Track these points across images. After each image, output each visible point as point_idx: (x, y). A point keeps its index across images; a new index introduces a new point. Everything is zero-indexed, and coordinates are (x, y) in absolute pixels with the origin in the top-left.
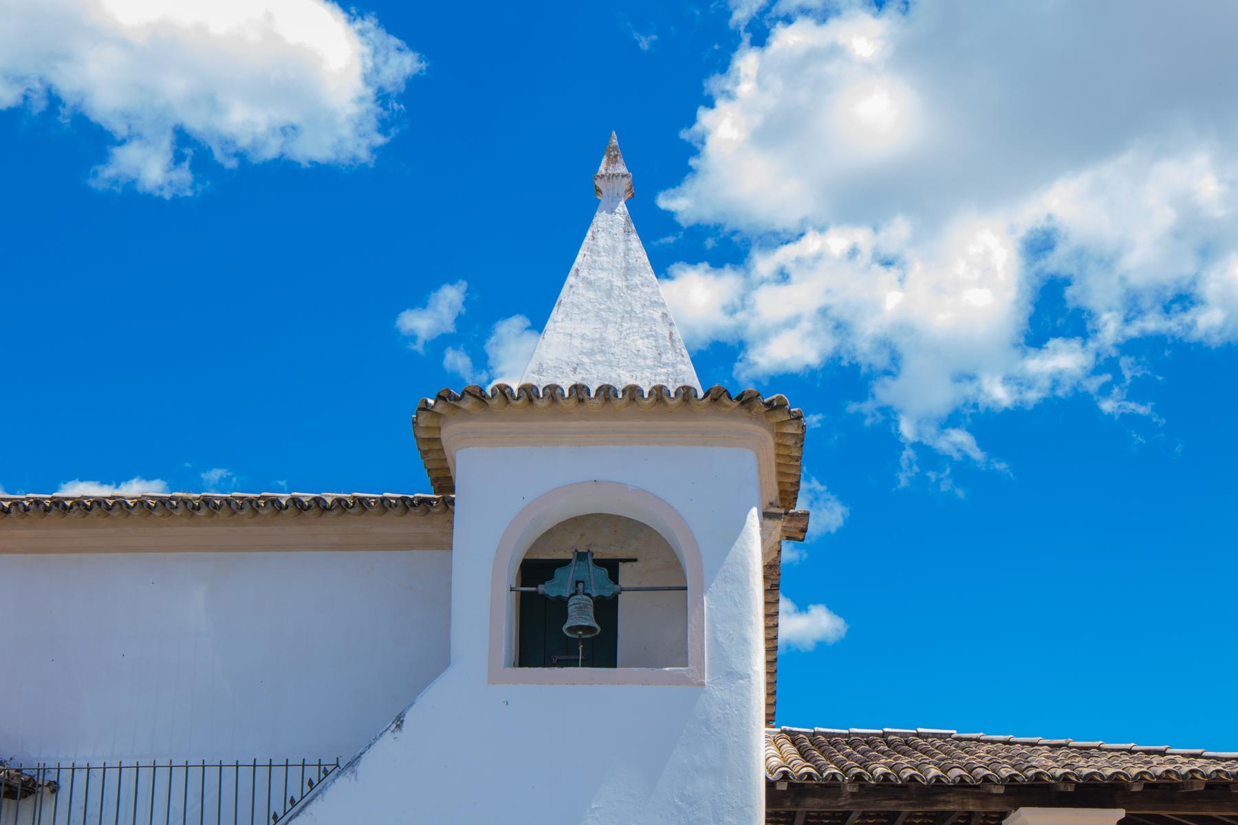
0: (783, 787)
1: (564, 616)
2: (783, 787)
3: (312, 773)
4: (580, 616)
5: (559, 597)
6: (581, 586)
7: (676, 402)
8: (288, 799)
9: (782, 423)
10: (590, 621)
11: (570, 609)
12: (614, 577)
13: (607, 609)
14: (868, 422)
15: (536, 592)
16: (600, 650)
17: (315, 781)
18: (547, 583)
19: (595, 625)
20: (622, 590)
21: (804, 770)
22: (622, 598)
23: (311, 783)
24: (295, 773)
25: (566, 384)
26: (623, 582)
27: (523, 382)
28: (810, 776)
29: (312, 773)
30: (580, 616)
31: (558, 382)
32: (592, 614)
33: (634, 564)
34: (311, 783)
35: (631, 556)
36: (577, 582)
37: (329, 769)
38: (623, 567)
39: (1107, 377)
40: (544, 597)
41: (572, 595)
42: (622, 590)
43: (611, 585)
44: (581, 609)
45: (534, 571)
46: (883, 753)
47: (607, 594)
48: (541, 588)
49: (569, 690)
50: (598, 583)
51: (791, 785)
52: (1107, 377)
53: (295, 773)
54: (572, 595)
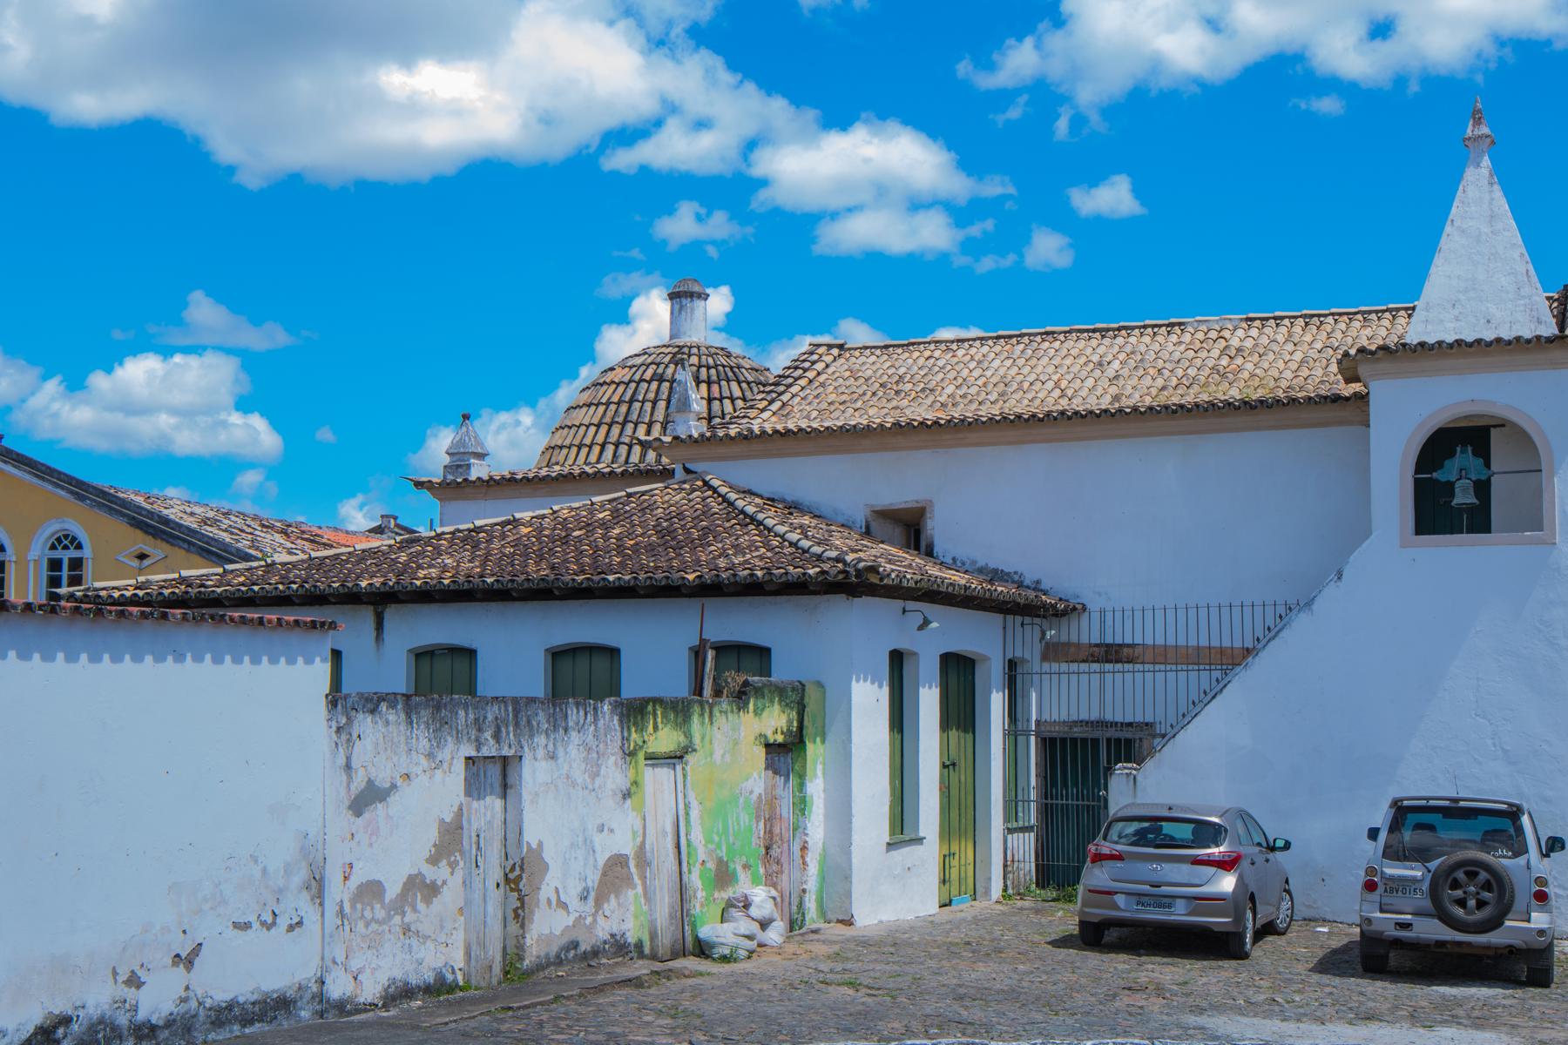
1: (1452, 495)
12: (1488, 465)
13: (1483, 489)
16: (1478, 520)
40: (1436, 481)
43: (1485, 471)
44: (1465, 490)
47: (1483, 478)
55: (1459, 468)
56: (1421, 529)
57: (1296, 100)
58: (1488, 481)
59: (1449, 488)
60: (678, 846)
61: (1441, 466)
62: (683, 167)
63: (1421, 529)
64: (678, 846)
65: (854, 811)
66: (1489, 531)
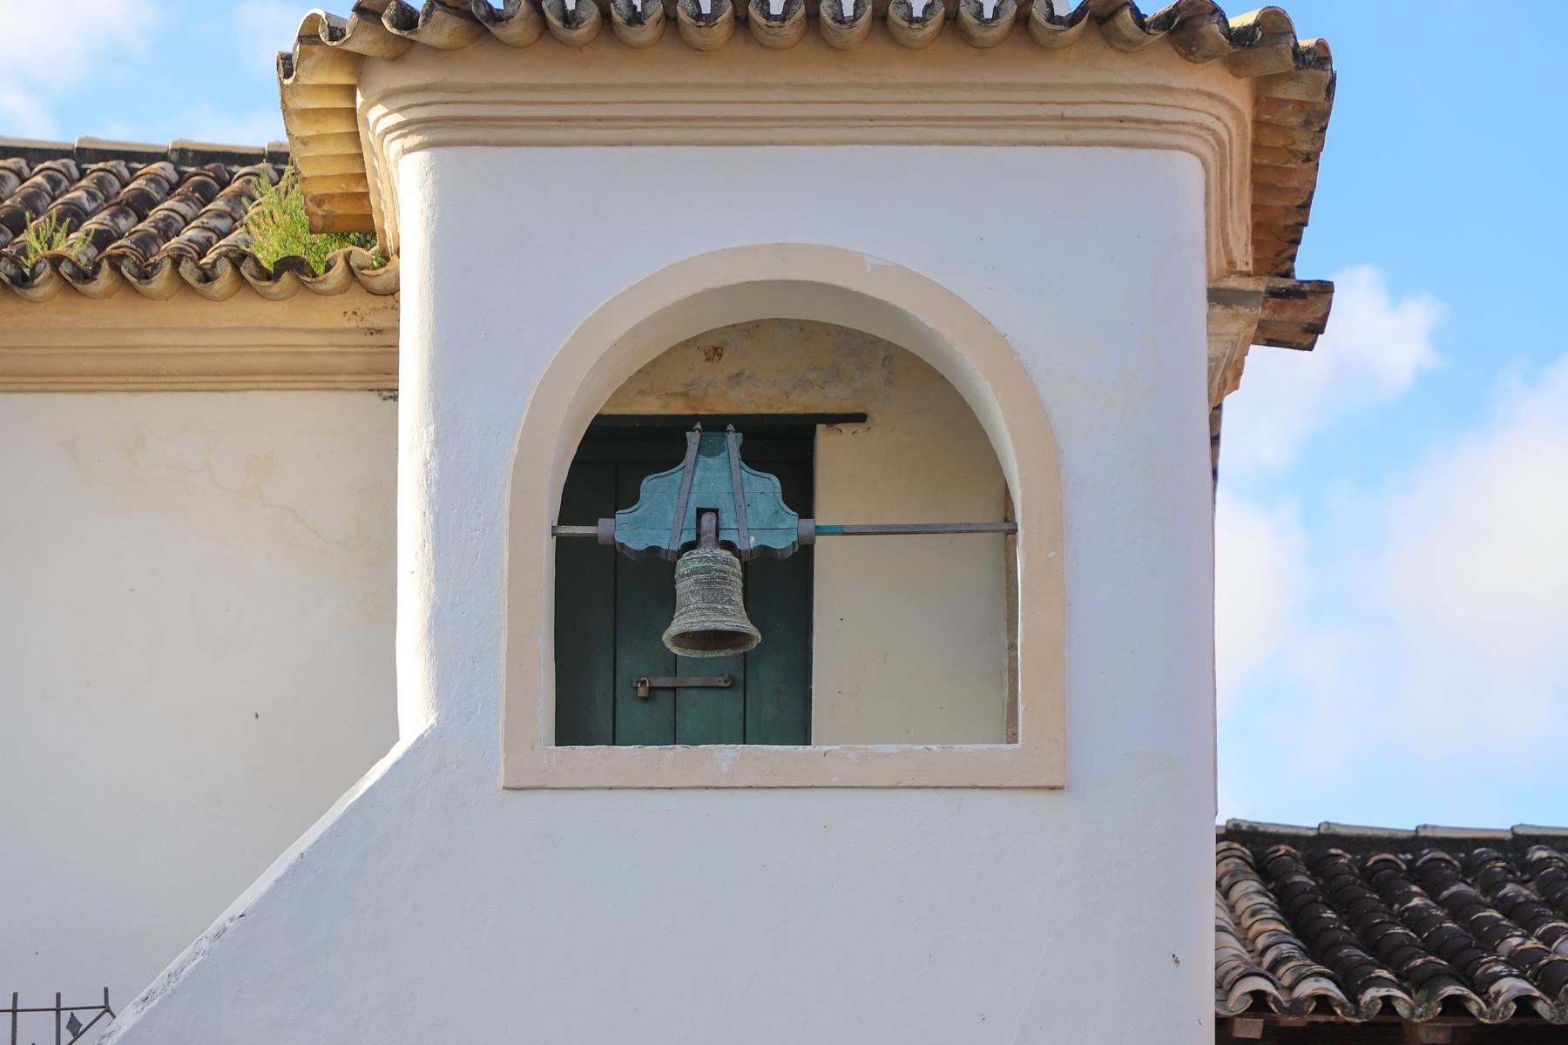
1: (667, 603)
2: (1252, 1029)
4: (705, 604)
5: (653, 550)
6: (708, 521)
7: (995, 32)
9: (1275, 79)
10: (736, 620)
11: (682, 587)
12: (800, 497)
13: (781, 587)
14: (371, 38)
16: (762, 681)
18: (621, 516)
19: (747, 627)
20: (820, 531)
21: (1307, 988)
26: (827, 510)
28: (1323, 1002)
30: (705, 604)
32: (738, 598)
36: (700, 512)
39: (244, 200)
40: (614, 551)
42: (820, 531)
43: (791, 519)
44: (712, 582)
45: (616, 455)
46: (1511, 909)
47: (781, 542)
51: (1271, 1029)
52: (244, 200)
55: (706, 505)
56: (573, 726)
57: (665, 636)
58: (805, 552)
59: (655, 574)
60: (1184, 123)
61: (630, 498)
62: (429, 336)
63: (573, 726)
64: (1184, 123)
65: (736, 281)
66: (807, 742)
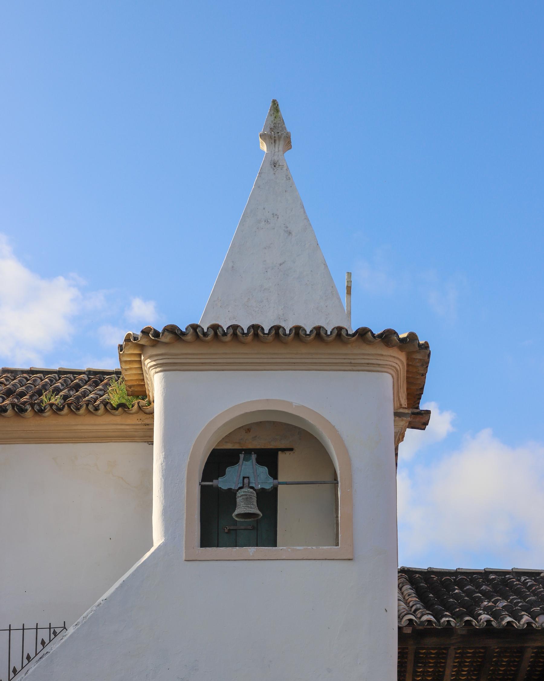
0: (409, 631)
1: (234, 505)
2: (409, 631)
3: (44, 635)
4: (246, 505)
5: (230, 489)
6: (246, 481)
8: (39, 641)
11: (238, 500)
12: (274, 473)
13: (268, 500)
15: (212, 486)
16: (263, 529)
17: (47, 641)
18: (220, 479)
21: (425, 618)
22: (280, 487)
23: (43, 643)
24: (30, 635)
25: (288, 326)
27: (254, 323)
29: (44, 635)
30: (246, 505)
31: (283, 324)
32: (255, 503)
33: (291, 452)
34: (43, 643)
35: (288, 446)
36: (244, 478)
37: (58, 631)
38: (282, 457)
40: (218, 489)
41: (241, 488)
43: (271, 480)
44: (248, 499)
45: (219, 461)
47: (268, 487)
48: (215, 483)
49: (241, 569)
50: (261, 477)
51: (414, 630)
53: (30, 635)
54: (241, 488)
